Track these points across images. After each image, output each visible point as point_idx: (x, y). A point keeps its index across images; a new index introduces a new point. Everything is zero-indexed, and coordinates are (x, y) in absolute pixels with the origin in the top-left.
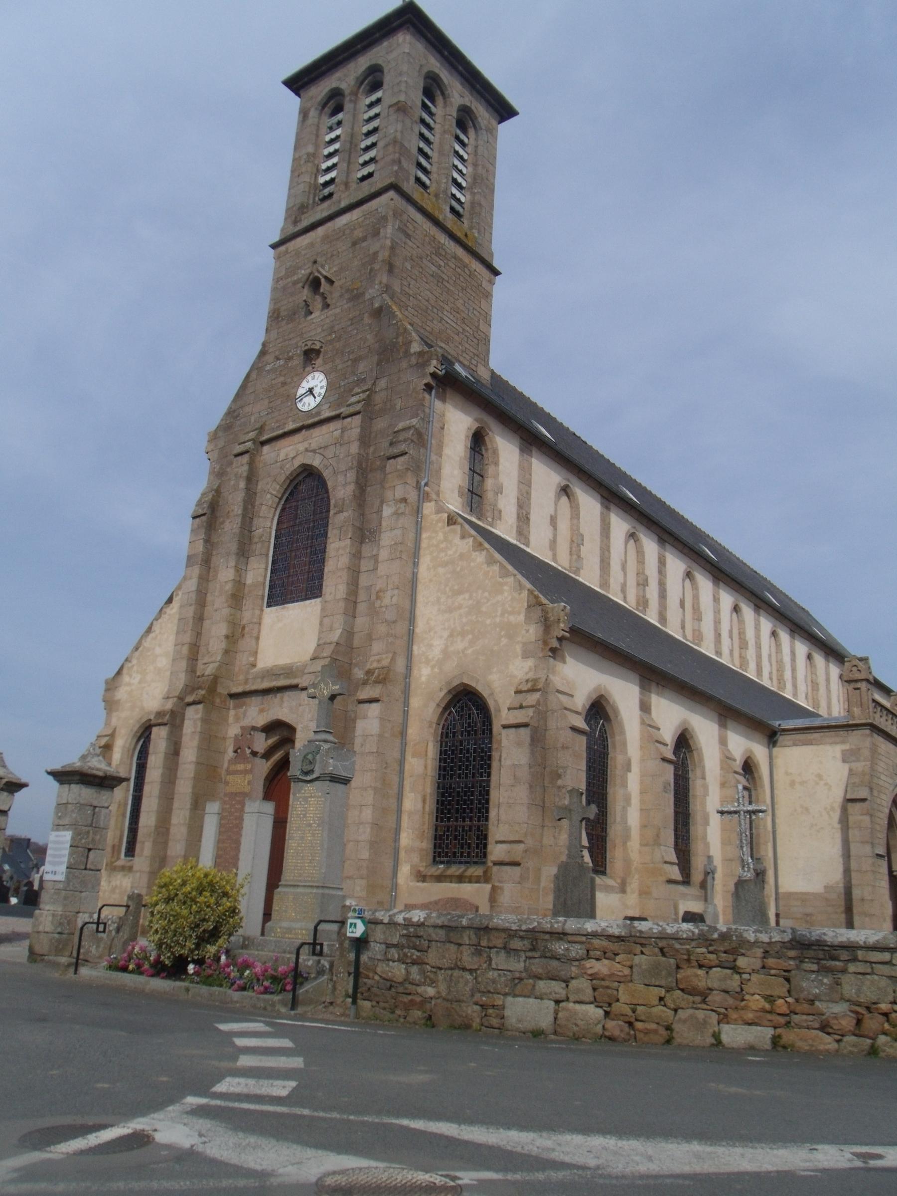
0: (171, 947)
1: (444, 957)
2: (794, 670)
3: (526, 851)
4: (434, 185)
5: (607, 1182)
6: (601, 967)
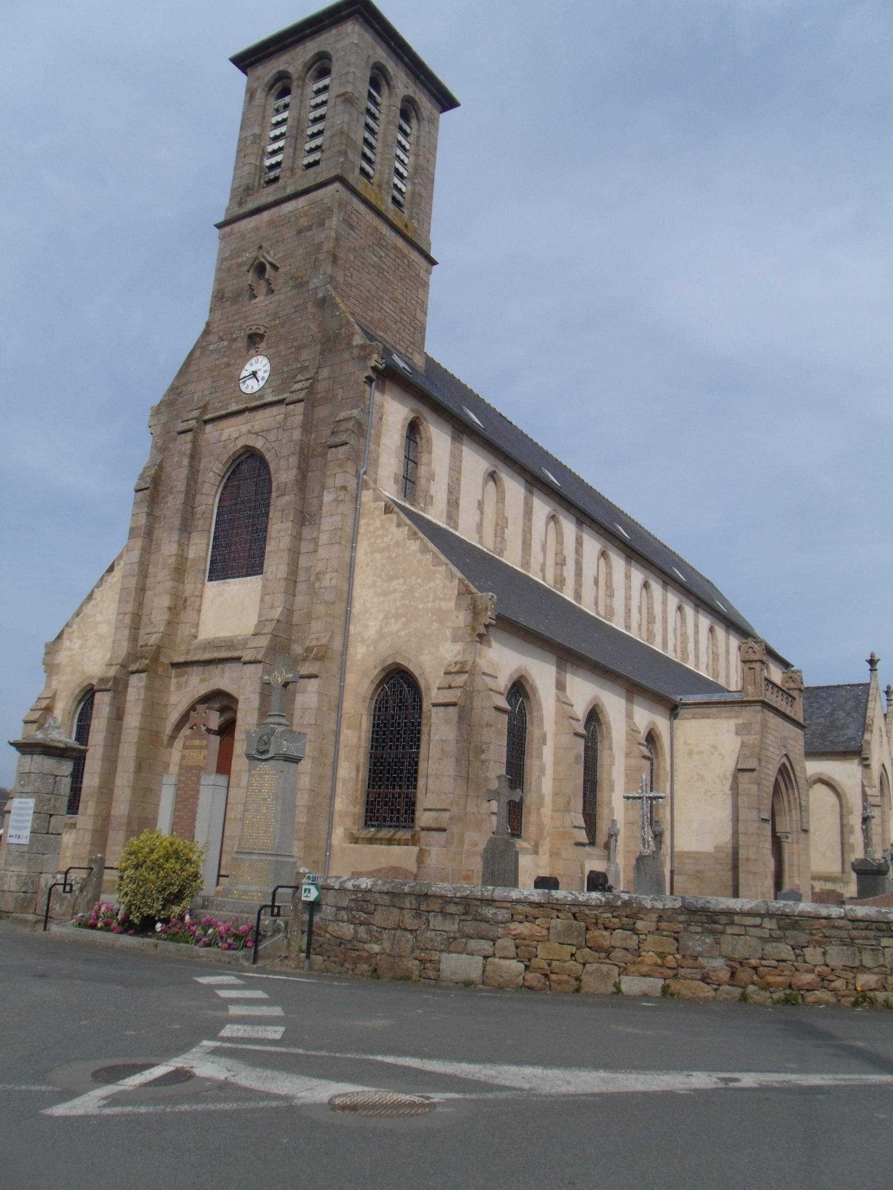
0: (140, 908)
1: (388, 919)
2: (696, 642)
3: (451, 819)
4: (378, 175)
5: (539, 1099)
6: (523, 929)
